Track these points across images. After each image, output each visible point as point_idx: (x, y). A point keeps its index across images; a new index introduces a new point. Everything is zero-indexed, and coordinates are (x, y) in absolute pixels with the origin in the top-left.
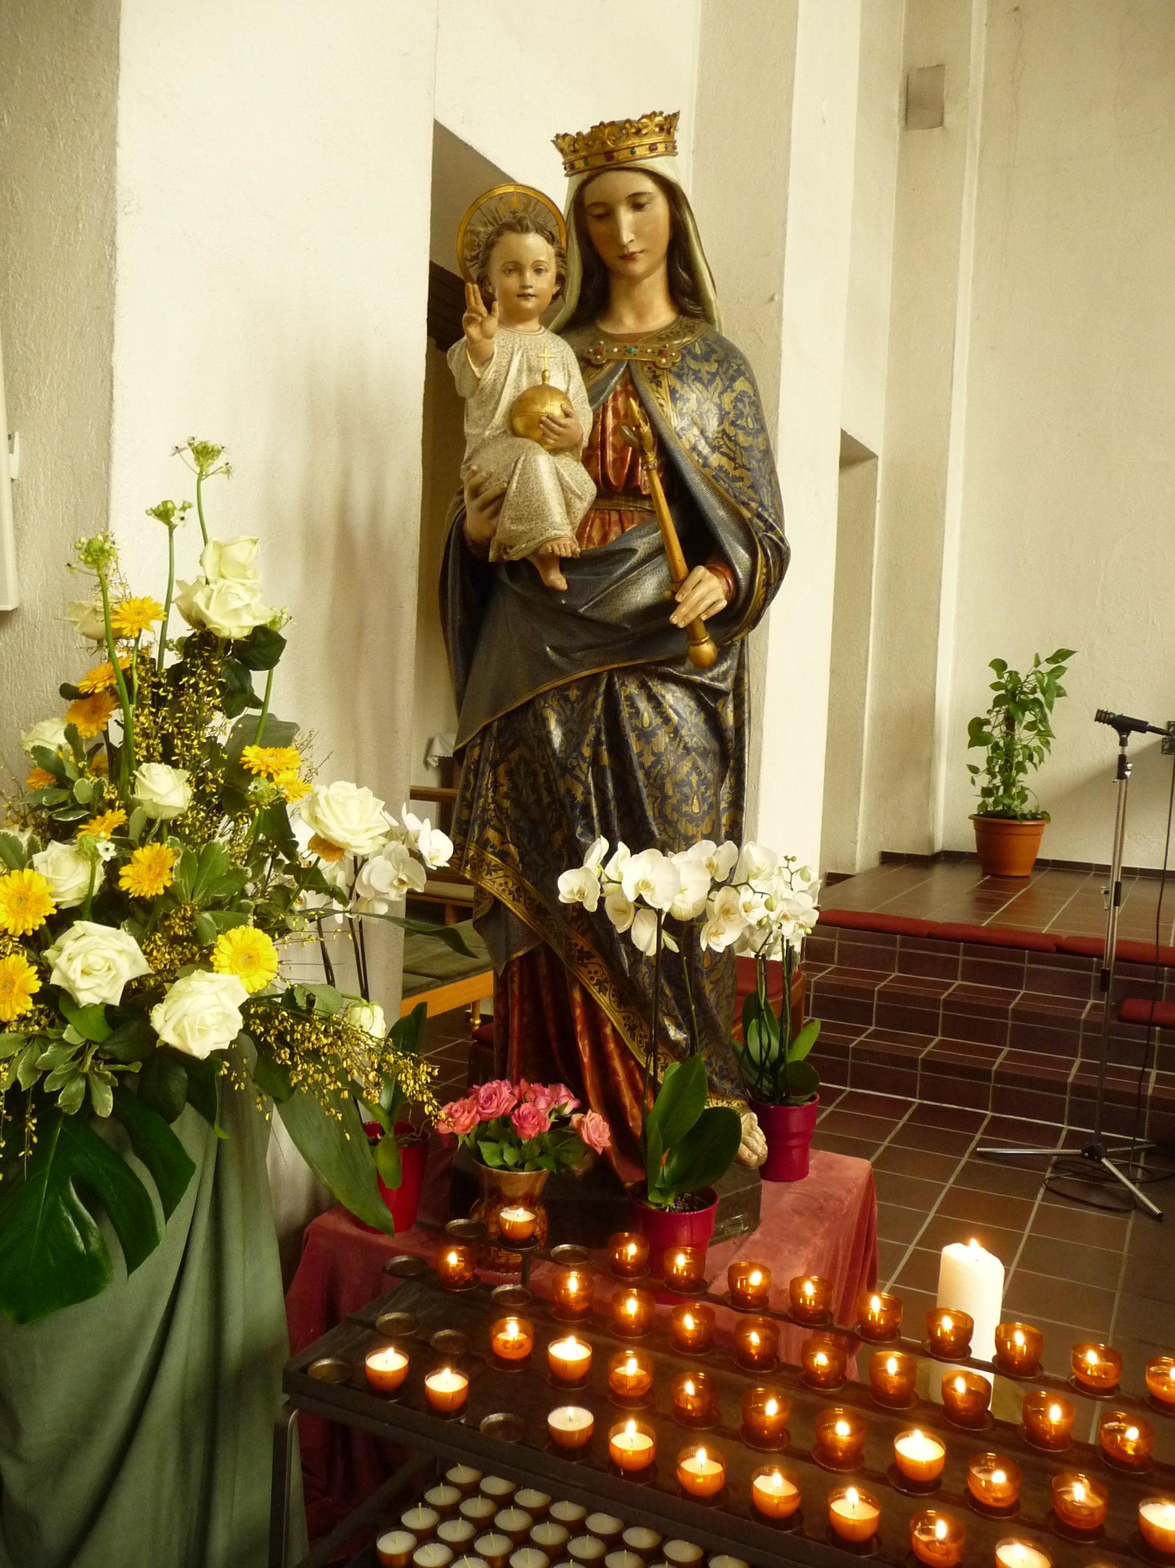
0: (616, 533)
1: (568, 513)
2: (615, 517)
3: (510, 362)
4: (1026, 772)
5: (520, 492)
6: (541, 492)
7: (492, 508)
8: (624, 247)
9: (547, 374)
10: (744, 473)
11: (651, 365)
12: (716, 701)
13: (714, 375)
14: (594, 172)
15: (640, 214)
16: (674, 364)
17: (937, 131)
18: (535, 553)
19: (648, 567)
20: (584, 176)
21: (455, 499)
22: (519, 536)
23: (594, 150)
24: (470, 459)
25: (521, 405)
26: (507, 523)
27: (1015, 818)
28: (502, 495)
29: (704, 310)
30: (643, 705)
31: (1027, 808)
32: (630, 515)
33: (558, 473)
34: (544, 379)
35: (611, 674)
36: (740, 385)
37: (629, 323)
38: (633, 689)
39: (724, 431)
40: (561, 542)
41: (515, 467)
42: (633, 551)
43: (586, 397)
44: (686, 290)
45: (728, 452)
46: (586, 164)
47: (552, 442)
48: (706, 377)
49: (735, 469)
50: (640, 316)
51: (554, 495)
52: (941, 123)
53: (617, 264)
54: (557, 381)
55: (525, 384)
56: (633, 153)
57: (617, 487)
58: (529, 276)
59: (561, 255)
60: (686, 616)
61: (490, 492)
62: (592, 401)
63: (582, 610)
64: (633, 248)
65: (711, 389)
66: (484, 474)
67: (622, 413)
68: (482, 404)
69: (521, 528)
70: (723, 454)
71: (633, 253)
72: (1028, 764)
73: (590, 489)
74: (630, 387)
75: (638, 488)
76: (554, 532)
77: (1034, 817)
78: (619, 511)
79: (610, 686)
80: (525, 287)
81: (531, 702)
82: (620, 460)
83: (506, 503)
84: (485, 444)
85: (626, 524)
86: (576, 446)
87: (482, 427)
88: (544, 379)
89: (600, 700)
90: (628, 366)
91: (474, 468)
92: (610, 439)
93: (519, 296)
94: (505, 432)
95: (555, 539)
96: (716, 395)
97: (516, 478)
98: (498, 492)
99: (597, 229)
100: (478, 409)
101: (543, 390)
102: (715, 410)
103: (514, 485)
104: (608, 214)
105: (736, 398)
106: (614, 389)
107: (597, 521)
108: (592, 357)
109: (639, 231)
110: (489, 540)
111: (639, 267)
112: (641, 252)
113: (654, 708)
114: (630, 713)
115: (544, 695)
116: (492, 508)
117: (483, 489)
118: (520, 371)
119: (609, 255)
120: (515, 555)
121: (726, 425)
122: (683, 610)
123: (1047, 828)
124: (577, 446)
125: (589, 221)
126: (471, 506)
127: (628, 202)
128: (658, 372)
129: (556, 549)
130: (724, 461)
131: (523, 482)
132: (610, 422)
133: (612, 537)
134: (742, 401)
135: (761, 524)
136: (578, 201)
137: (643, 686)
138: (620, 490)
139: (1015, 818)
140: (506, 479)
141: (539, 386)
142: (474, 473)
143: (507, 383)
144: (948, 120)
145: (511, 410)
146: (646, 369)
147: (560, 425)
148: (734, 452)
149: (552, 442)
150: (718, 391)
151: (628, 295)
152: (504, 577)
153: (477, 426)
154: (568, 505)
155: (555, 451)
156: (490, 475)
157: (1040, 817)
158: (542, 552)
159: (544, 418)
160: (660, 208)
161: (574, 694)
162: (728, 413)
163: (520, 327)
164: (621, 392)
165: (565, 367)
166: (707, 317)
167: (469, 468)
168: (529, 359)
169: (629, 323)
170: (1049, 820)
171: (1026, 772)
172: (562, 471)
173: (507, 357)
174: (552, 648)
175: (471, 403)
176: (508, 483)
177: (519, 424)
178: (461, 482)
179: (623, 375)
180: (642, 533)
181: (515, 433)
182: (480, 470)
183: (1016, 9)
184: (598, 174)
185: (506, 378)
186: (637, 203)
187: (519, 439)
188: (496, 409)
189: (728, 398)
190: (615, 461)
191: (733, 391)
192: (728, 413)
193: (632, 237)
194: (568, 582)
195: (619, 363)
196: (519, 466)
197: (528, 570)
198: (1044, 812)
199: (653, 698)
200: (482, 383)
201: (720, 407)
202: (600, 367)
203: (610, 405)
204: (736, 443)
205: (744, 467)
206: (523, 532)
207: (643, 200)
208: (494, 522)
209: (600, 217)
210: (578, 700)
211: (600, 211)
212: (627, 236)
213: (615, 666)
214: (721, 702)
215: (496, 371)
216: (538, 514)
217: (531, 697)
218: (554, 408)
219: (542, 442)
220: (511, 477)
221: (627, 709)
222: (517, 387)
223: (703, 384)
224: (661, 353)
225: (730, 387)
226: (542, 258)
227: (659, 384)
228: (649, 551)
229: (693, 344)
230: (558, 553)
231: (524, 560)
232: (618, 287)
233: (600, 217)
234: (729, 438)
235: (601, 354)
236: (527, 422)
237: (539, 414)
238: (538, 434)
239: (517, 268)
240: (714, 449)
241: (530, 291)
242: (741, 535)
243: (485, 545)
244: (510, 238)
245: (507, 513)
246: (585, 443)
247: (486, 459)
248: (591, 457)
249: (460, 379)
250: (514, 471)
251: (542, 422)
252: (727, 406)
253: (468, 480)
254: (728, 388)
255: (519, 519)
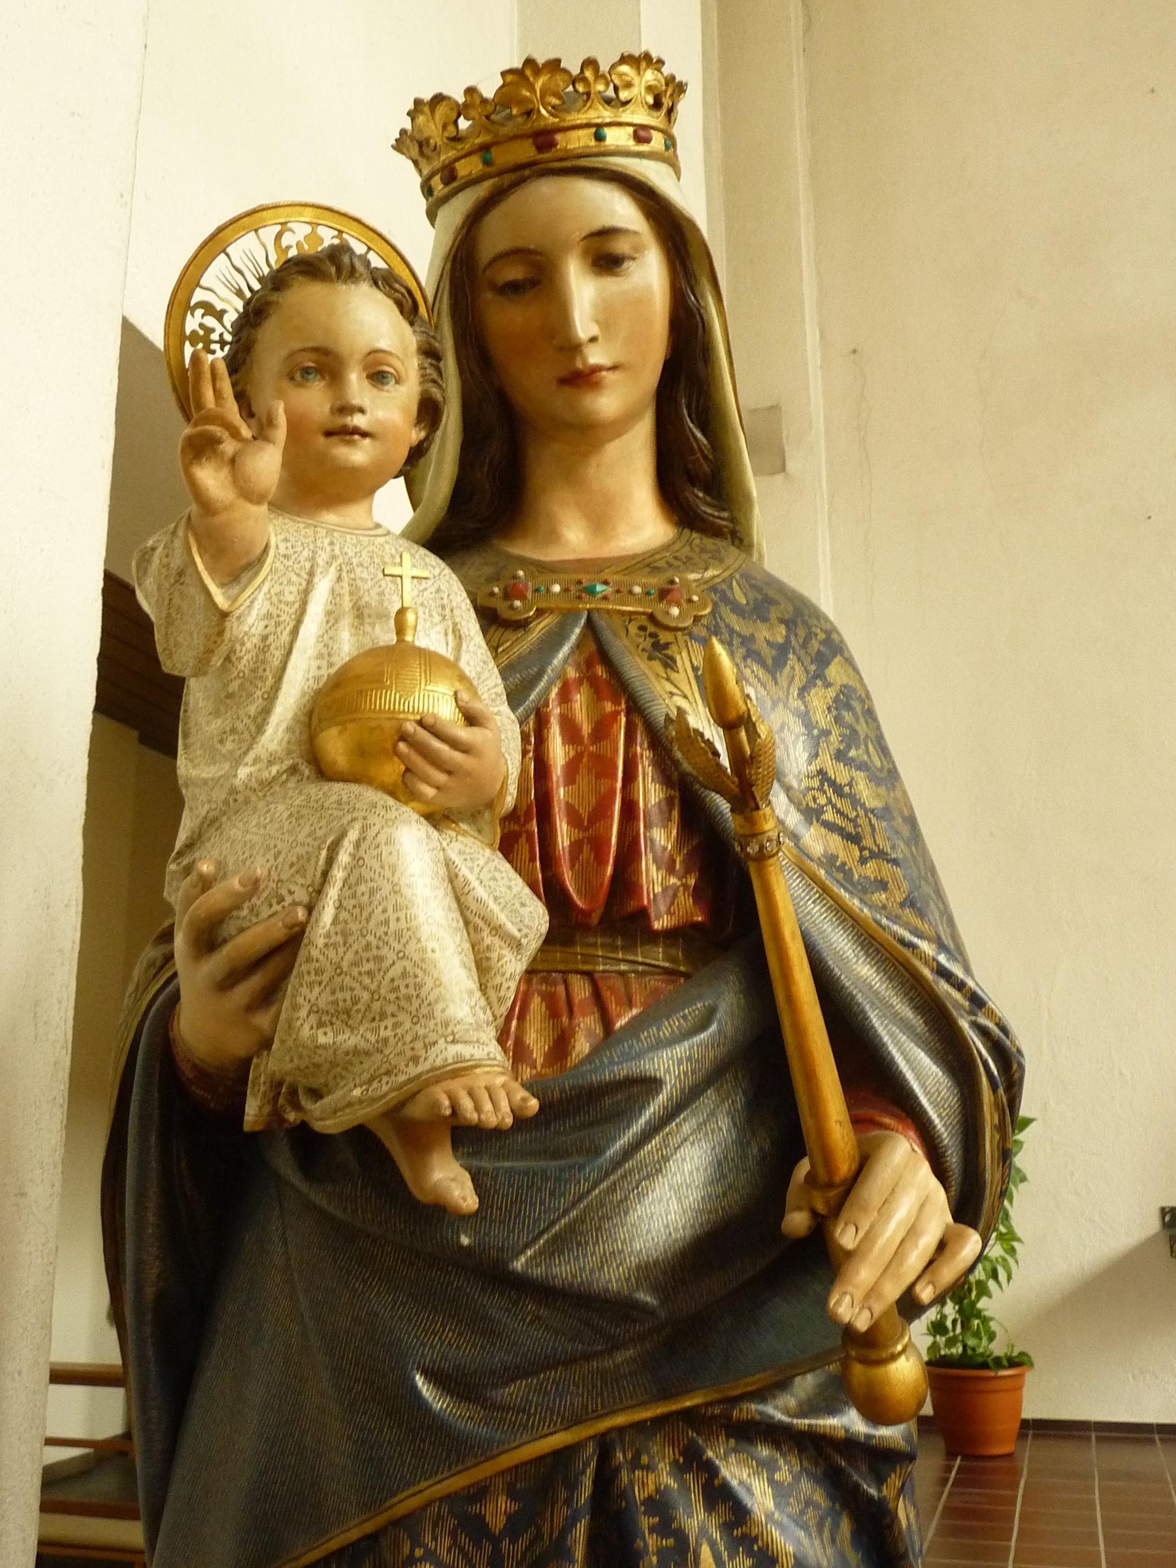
0: (590, 1033)
1: (483, 988)
2: (581, 990)
3: (306, 593)
4: (990, 1296)
5: (345, 934)
6: (406, 935)
7: (256, 982)
8: (574, 348)
9: (410, 617)
10: (887, 870)
11: (643, 620)
12: (880, 1480)
13: (783, 650)
14: (508, 179)
15: (611, 285)
16: (697, 619)
17: (779, 478)
18: (395, 1114)
19: (686, 1124)
20: (481, 191)
21: (151, 953)
22: (344, 1063)
23: (508, 129)
24: (190, 846)
25: (337, 698)
26: (306, 1024)
27: (984, 1366)
28: (292, 942)
29: (732, 520)
30: (696, 1520)
31: (998, 1348)
32: (618, 983)
33: (452, 878)
34: (400, 630)
35: (605, 1444)
36: (835, 671)
37: (574, 538)
38: (662, 1476)
39: (821, 773)
40: (480, 1080)
41: (330, 861)
42: (651, 1084)
43: (501, 689)
44: (698, 477)
45: (839, 821)
46: (487, 163)
47: (430, 792)
48: (768, 653)
49: (863, 861)
50: (600, 520)
51: (439, 934)
52: (783, 468)
53: (558, 401)
54: (429, 636)
55: (346, 646)
56: (599, 138)
57: (586, 914)
58: (356, 385)
59: (430, 353)
60: (873, 1292)
61: (255, 933)
62: (514, 698)
63: (519, 1264)
64: (595, 356)
65: (783, 679)
66: (235, 883)
67: (586, 729)
68: (226, 700)
69: (348, 1039)
70: (830, 826)
71: (597, 369)
72: (991, 1284)
73: (533, 918)
74: (600, 671)
75: (642, 915)
76: (453, 1050)
77: (1013, 1363)
78: (589, 975)
79: (606, 1478)
80: (346, 409)
81: (373, 1538)
82: (590, 842)
83: (301, 966)
84: (236, 802)
85: (613, 1007)
86: (490, 805)
87: (227, 758)
88: (400, 630)
89: (581, 1530)
90: (590, 624)
91: (206, 867)
92: (561, 794)
93: (329, 434)
94: (293, 770)
95: (456, 1073)
96: (795, 692)
97: (333, 893)
98: (277, 931)
99: (506, 319)
100: (216, 713)
101: (398, 657)
102: (797, 727)
103: (327, 915)
104: (537, 278)
105: (836, 700)
106: (561, 675)
107: (536, 1004)
108: (501, 607)
109: (612, 316)
110: (245, 1064)
111: (607, 403)
112: (614, 368)
113: (727, 1527)
114: (660, 1552)
115: (409, 1523)
116: (256, 982)
117: (230, 927)
118: (332, 616)
119: (532, 383)
120: (327, 1118)
121: (826, 761)
122: (863, 1274)
123: (1030, 1378)
124: (490, 805)
125: (489, 302)
126: (194, 977)
127: (586, 253)
128: (664, 637)
129: (467, 1104)
130: (835, 843)
131: (356, 905)
132: (558, 752)
133: (582, 1046)
134: (849, 708)
135: (956, 995)
136: (462, 262)
137: (693, 1463)
138: (595, 920)
139: (984, 1366)
140: (302, 896)
141: (389, 649)
142: (206, 884)
143: (299, 644)
144: (790, 466)
145: (310, 714)
146: (633, 629)
147: (455, 744)
148: (853, 821)
149: (430, 792)
150: (797, 683)
151: (571, 475)
152: (284, 1163)
153: (213, 757)
154: (483, 967)
155: (438, 818)
156: (254, 885)
157: (1018, 1362)
158: (417, 1110)
159: (410, 727)
160: (650, 272)
161: (498, 1511)
162: (826, 733)
163: (330, 517)
164: (580, 682)
165: (445, 612)
166: (736, 535)
167: (188, 870)
168: (351, 583)
169: (574, 538)
170: (1032, 1365)
171: (990, 1296)
172: (464, 871)
173: (299, 582)
174: (432, 1376)
175: (198, 697)
176: (310, 909)
177: (335, 745)
178: (168, 910)
179: (579, 646)
180: (666, 1032)
181: (323, 772)
182: (222, 870)
183: (854, 351)
184: (523, 181)
185: (295, 632)
186: (605, 257)
187: (337, 787)
188: (266, 711)
189: (820, 700)
190: (576, 847)
191: (828, 685)
192: (826, 733)
193: (594, 330)
194: (478, 1187)
195: (568, 617)
196: (343, 857)
197: (369, 1160)
198: (1022, 1354)
199: (720, 1497)
200: (234, 629)
201: (808, 724)
202: (522, 625)
203: (555, 711)
204: (855, 801)
205: (880, 855)
206: (356, 1052)
207: (622, 246)
208: (262, 1020)
209: (514, 288)
210: (514, 1527)
211: (515, 272)
212: (583, 325)
213: (620, 1420)
214: (894, 1481)
215: (268, 616)
216: (405, 997)
217: (369, 1527)
218: (438, 701)
219: (403, 791)
220: (319, 891)
221: (652, 1541)
222: (326, 653)
223: (762, 663)
224: (664, 594)
225: (820, 675)
226: (383, 344)
227: (669, 664)
228: (689, 1082)
229: (728, 581)
230: (471, 1116)
231: (360, 1136)
232: (543, 463)
233: (514, 288)
234: (838, 790)
235: (522, 597)
236: (357, 738)
237: (392, 714)
238: (391, 770)
239: (325, 364)
240: (811, 814)
241: (358, 421)
242: (917, 1022)
243: (235, 1078)
244: (307, 295)
245: (304, 996)
246: (510, 801)
247: (243, 830)
248: (522, 834)
249: (169, 621)
250: (325, 874)
251: (403, 737)
252: (822, 719)
253: (189, 901)
254: (817, 677)
255: (344, 1015)
